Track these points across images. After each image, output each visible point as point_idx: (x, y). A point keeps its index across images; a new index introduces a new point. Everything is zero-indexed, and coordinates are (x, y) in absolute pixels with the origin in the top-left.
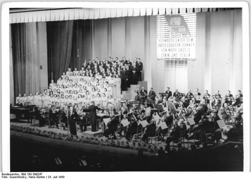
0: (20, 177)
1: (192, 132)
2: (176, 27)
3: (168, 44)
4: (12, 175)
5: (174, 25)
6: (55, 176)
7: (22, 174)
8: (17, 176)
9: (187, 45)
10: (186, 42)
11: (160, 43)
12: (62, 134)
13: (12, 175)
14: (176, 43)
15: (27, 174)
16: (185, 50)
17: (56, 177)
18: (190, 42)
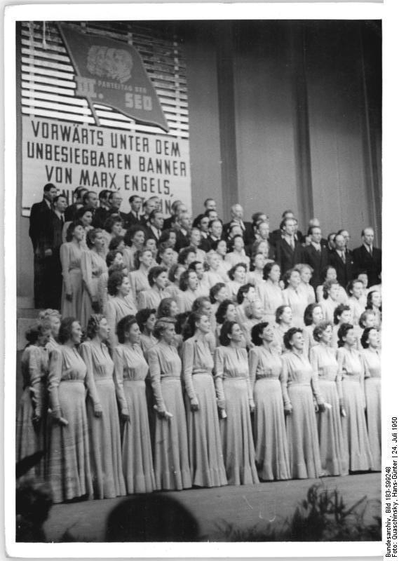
0: (395, 517)
1: (355, 277)
2: (115, 86)
3: (79, 153)
4: (389, 534)
5: (105, 78)
6: (393, 438)
7: (388, 511)
8: (392, 522)
9: (159, 166)
10: (151, 154)
11: (40, 140)
12: (246, 531)
13: (389, 534)
14: (116, 151)
15: (388, 502)
16: (152, 185)
17: (395, 435)
18: (171, 158)
